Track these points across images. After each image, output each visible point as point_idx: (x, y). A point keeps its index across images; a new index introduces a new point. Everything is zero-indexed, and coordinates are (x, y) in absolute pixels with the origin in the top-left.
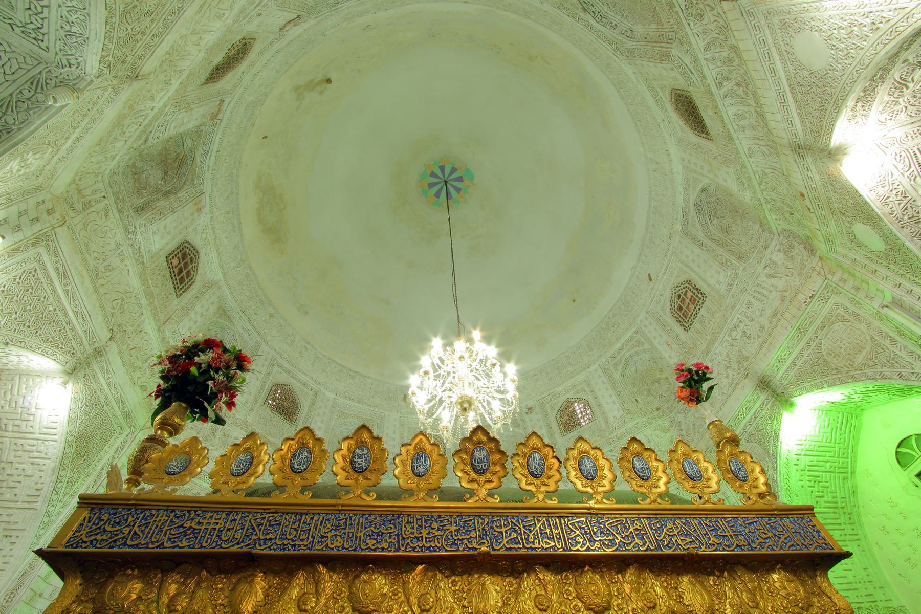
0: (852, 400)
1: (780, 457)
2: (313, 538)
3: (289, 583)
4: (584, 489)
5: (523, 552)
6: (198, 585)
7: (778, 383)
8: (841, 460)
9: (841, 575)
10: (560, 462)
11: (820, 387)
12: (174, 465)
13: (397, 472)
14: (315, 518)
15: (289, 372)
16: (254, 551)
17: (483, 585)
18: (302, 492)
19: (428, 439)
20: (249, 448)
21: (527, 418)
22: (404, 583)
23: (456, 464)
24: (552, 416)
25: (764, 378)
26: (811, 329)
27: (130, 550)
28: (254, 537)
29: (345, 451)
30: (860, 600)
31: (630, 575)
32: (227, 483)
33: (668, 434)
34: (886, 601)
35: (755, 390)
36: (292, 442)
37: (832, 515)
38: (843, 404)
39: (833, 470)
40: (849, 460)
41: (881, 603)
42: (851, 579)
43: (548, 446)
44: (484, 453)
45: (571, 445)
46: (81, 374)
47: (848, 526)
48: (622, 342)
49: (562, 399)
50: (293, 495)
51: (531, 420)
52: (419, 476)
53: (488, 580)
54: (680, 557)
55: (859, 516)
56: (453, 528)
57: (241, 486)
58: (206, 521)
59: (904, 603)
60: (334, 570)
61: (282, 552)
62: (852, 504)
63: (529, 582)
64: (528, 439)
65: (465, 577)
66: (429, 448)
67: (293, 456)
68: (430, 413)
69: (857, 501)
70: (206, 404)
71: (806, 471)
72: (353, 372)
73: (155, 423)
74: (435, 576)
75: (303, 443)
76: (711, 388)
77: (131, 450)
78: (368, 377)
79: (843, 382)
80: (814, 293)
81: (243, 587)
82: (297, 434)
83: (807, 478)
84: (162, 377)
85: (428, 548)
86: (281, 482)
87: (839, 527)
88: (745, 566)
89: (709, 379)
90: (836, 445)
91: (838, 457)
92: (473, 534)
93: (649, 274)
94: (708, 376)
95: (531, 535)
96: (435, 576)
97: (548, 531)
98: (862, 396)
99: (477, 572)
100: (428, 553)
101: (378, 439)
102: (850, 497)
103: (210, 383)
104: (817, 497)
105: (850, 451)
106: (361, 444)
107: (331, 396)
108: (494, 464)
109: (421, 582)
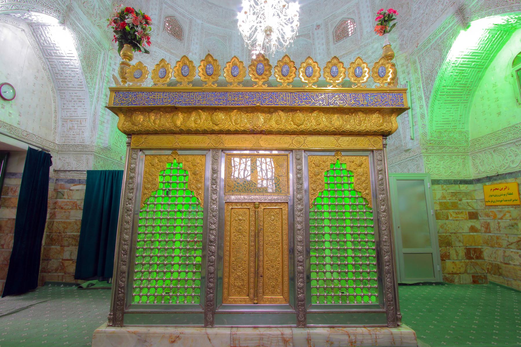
0: (510, 23)
2: (195, 101)
3: (190, 115)
4: (305, 81)
5: (273, 106)
6: (161, 116)
7: (468, 11)
10: (296, 69)
11: (489, 14)
12: (137, 74)
13: (225, 75)
14: (195, 94)
15: (172, 7)
16: (176, 106)
17: (258, 116)
18: (188, 84)
19: (238, 59)
20: (163, 66)
21: (315, 32)
22: (230, 116)
23: (250, 71)
24: (331, 30)
25: (462, 6)
27: (134, 106)
28: (175, 101)
29: (202, 67)
31: (315, 114)
32: (159, 81)
33: (394, 43)
35: (453, 15)
36: (180, 63)
38: (504, 26)
43: (292, 61)
44: (261, 66)
45: (304, 61)
46: (68, 23)
49: (340, 18)
50: (185, 85)
51: (318, 34)
52: (234, 76)
53: (259, 114)
54: (336, 108)
56: (247, 97)
57: (165, 82)
58: (156, 96)
60: (205, 112)
61: (185, 106)
63: (275, 116)
64: (283, 58)
65: (251, 114)
66: (238, 63)
67: (182, 69)
68: (250, 37)
70: (138, 45)
72: (210, 3)
73: (121, 55)
74: (240, 114)
75: (185, 63)
76: (394, 25)
77: (117, 68)
78: (221, 7)
81: (175, 117)
82: (181, 59)
84: (114, 31)
85: (238, 104)
86: (179, 80)
88: (363, 112)
89: (394, 19)
92: (255, 99)
94: (394, 17)
95: (278, 100)
96: (240, 114)
97: (285, 98)
98: (516, 20)
99: (256, 112)
100: (237, 106)
101: (216, 60)
103: (136, 33)
106: (209, 63)
107: (199, 22)
108: (266, 71)
109: (236, 115)
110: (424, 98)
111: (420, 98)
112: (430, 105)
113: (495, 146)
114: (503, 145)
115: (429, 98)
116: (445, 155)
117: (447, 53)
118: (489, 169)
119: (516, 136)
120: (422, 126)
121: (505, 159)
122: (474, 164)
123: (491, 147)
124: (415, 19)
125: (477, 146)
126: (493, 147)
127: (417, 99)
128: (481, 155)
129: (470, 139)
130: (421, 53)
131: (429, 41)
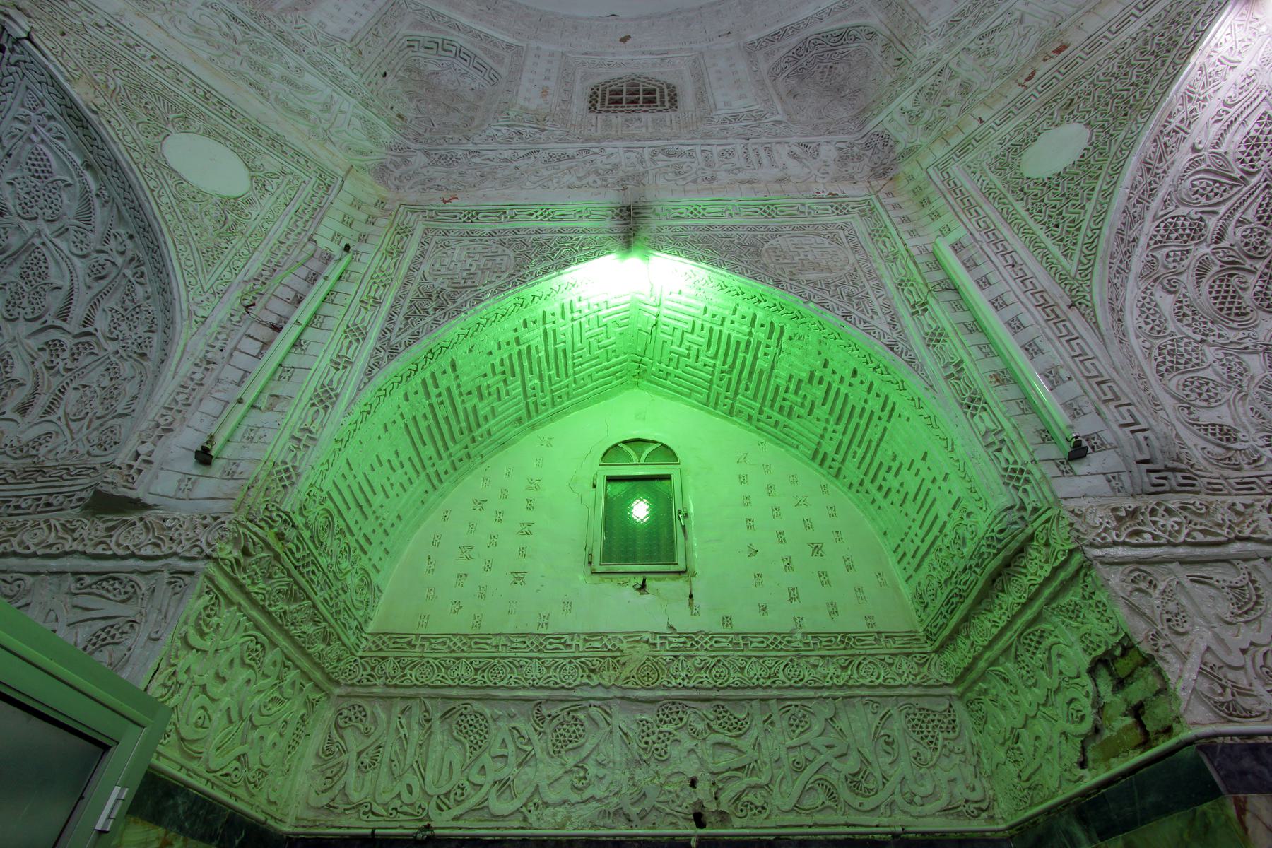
8: (548, 398)
9: (374, 485)
25: (644, 207)
30: (355, 529)
35: (611, 209)
37: (456, 429)
39: (529, 395)
40: (551, 411)
41: (367, 561)
48: (474, 26)
55: (470, 471)
59: (387, 589)
71: (516, 349)
80: (840, 194)
83: (506, 356)
91: (552, 391)
93: (629, 37)
102: (494, 442)
104: (479, 388)
110: (371, 342)
111: (358, 333)
112: (380, 379)
113: (462, 693)
114: (494, 698)
115: (394, 354)
116: (274, 645)
117: (545, 272)
118: (386, 797)
119: (556, 676)
120: (298, 435)
122: (327, 752)
126: (454, 692)
127: (343, 327)
128: (383, 715)
130: (445, 226)
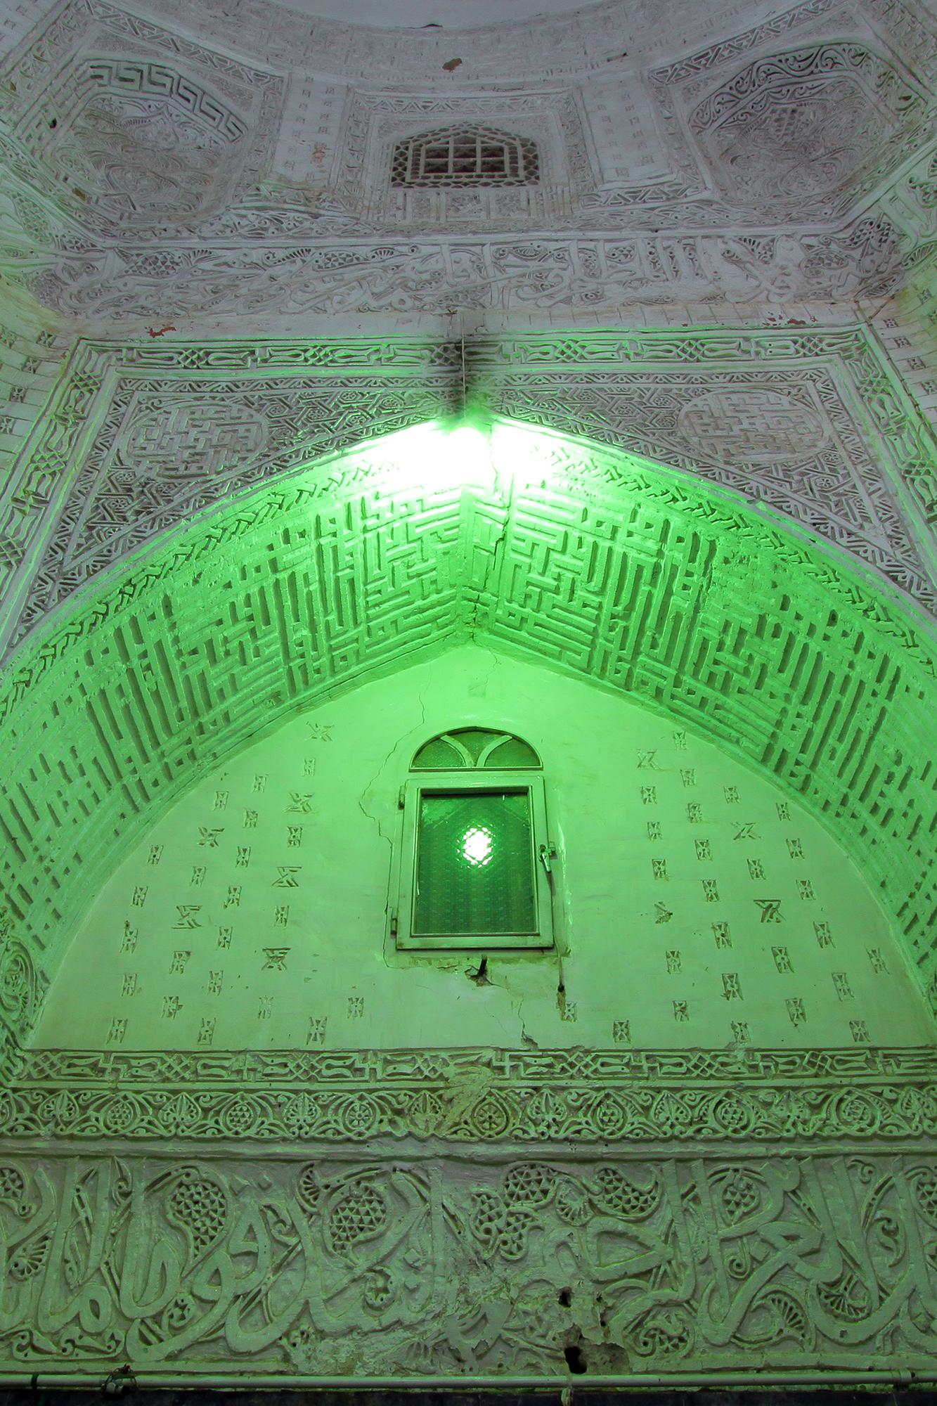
1: (300, 473)
8: (325, 660)
9: (36, 804)
25: (484, 344)
26: (710, 365)
33: (26, 238)
34: (36, 938)
37: (172, 712)
40: (330, 681)
41: (25, 931)
42: (41, 830)
47: (159, 767)
55: (194, 780)
59: (56, 977)
62: (218, 750)
69: (229, 757)
71: (272, 578)
79: (669, 459)
80: (809, 322)
83: (254, 590)
87: (148, 744)
90: (362, 628)
91: (331, 649)
102: (235, 732)
104: (210, 644)
105: (354, 669)
110: (32, 566)
112: (46, 628)
113: (183, 1148)
115: (68, 586)
117: (320, 450)
118: (56, 1322)
119: (337, 1121)
121: (204, 1275)
123: (154, 1147)
124: (206, 254)
125: (60, 1107)
126: (169, 1148)
128: (50, 1186)
129: (30, 1041)
130: (153, 375)
131: (245, 354)
